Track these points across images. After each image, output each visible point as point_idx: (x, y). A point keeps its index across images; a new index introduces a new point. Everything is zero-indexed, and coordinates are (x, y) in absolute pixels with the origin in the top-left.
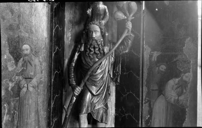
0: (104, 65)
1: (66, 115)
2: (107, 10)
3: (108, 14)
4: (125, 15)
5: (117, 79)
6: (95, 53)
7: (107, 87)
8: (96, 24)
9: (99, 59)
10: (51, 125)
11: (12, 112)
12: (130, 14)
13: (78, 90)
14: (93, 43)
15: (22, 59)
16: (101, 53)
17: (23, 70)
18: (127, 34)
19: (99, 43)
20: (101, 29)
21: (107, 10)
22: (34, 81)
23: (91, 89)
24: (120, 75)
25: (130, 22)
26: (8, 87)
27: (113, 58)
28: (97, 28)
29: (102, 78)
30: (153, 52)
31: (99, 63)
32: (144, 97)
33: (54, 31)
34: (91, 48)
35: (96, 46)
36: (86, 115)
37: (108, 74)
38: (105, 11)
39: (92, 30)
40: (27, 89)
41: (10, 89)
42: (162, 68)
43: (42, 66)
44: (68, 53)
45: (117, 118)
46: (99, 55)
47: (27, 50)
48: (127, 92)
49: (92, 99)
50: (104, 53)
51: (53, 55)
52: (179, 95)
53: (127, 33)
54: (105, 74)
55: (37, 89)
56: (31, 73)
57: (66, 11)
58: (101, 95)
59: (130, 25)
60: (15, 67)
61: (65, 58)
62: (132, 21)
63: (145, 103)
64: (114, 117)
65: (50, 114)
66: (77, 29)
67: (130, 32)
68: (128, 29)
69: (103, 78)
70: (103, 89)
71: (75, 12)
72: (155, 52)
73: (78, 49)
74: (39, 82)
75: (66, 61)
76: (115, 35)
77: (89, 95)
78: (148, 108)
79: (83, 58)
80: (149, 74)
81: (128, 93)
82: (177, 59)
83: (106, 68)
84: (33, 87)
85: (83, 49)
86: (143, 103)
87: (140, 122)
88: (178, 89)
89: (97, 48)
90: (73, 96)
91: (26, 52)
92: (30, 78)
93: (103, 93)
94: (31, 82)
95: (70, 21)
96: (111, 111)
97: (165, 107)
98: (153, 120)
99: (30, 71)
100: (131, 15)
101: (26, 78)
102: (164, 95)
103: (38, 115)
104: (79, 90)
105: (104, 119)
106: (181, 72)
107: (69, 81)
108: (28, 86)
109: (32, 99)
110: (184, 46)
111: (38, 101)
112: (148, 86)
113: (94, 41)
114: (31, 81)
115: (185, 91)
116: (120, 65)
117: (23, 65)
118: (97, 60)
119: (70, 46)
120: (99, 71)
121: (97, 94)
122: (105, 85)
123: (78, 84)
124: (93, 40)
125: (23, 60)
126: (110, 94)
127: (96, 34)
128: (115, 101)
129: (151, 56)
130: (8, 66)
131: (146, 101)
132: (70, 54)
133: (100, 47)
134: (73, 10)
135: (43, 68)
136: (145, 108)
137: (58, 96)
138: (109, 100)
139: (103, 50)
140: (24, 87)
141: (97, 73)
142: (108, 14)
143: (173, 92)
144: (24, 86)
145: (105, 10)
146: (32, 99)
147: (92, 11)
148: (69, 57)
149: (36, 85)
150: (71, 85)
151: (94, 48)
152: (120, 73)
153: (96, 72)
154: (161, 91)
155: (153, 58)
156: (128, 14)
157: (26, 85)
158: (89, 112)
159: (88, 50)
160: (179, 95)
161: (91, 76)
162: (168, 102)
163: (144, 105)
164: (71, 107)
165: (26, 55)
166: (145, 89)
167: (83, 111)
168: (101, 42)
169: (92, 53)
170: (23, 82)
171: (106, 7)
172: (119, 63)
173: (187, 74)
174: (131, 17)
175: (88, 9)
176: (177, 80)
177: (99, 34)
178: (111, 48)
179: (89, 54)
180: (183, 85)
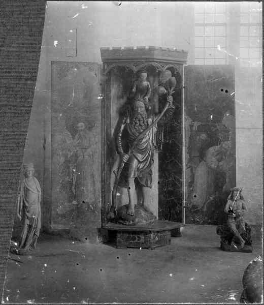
2: (150, 87)
4: (167, 89)
5: (160, 146)
9: (144, 130)
12: (171, 88)
16: (145, 125)
19: (143, 116)
38: (148, 85)
47: (82, 126)
50: (148, 125)
52: (219, 161)
55: (92, 157)
59: (170, 99)
60: (72, 141)
62: (173, 95)
66: (123, 101)
68: (170, 102)
71: (119, 85)
72: (196, 122)
73: (124, 121)
77: (135, 161)
80: (186, 79)
91: (80, 129)
92: (86, 149)
100: (172, 89)
102: (205, 161)
107: (117, 150)
113: (139, 116)
118: (142, 131)
120: (144, 140)
123: (126, 152)
124: (138, 115)
139: (147, 122)
140: (80, 156)
141: (142, 142)
145: (148, 85)
148: (115, 127)
150: (119, 153)
153: (141, 142)
154: (202, 156)
156: (169, 89)
158: (136, 176)
160: (219, 161)
161: (137, 145)
169: (137, 125)
173: (226, 142)
174: (172, 92)
177: (143, 109)
180: (221, 155)
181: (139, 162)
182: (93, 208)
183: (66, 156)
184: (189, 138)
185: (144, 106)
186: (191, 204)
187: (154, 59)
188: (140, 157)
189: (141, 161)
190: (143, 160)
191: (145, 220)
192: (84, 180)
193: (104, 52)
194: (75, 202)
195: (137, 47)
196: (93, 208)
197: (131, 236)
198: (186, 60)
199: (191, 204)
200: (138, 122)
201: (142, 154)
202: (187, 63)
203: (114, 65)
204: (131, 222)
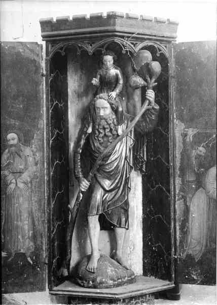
0: (119, 150)
1: (72, 216)
2: (120, 76)
3: (121, 82)
4: (146, 80)
6: (105, 134)
7: (126, 180)
10: (52, 230)
13: (85, 185)
14: (101, 123)
15: (7, 151)
19: (110, 122)
21: (120, 76)
22: (26, 176)
23: (102, 183)
24: (145, 161)
25: (152, 91)
27: (132, 140)
29: (117, 166)
30: (187, 130)
32: (177, 191)
33: (50, 112)
34: (99, 130)
35: (107, 126)
36: (98, 216)
37: (126, 161)
38: (117, 75)
40: (15, 185)
43: (36, 157)
45: (146, 221)
46: (110, 138)
47: (13, 139)
48: (156, 184)
50: (118, 135)
51: (51, 142)
53: (148, 105)
55: (30, 185)
56: (20, 167)
57: (69, 74)
58: (116, 190)
61: (70, 142)
62: (154, 89)
63: (178, 200)
65: (50, 216)
66: (85, 101)
67: (153, 103)
68: (149, 100)
69: (118, 167)
71: (81, 79)
75: (72, 145)
78: (182, 206)
79: (91, 142)
81: (157, 186)
84: (24, 183)
85: (90, 130)
86: (176, 200)
90: (79, 193)
91: (12, 142)
93: (120, 187)
94: (20, 177)
96: (137, 211)
98: (190, 222)
99: (19, 164)
100: (153, 80)
102: (204, 189)
104: (87, 184)
108: (18, 181)
109: (23, 196)
111: (31, 200)
112: (183, 175)
114: (20, 176)
116: (145, 147)
120: (112, 158)
121: (110, 188)
122: (122, 176)
125: (9, 151)
129: (185, 135)
132: (77, 135)
133: (112, 128)
134: (79, 75)
135: (37, 159)
136: (179, 206)
137: (60, 192)
140: (11, 183)
142: (121, 82)
144: (12, 181)
145: (117, 75)
146: (23, 196)
149: (29, 180)
152: (145, 159)
154: (200, 183)
155: (188, 137)
156: (149, 79)
157: (14, 181)
159: (97, 132)
165: (12, 146)
166: (178, 181)
168: (113, 121)
169: (101, 135)
171: (118, 72)
172: (143, 144)
174: (153, 83)
179: (98, 137)
181: (106, 191)
182: (31, 262)
184: (181, 153)
185: (108, 106)
186: (185, 253)
187: (115, 31)
188: (107, 184)
189: (107, 189)
190: (112, 187)
191: (111, 280)
192: (17, 221)
196: (31, 262)
198: (174, 35)
199: (185, 253)
201: (109, 179)
203: (61, 45)
204: (91, 282)
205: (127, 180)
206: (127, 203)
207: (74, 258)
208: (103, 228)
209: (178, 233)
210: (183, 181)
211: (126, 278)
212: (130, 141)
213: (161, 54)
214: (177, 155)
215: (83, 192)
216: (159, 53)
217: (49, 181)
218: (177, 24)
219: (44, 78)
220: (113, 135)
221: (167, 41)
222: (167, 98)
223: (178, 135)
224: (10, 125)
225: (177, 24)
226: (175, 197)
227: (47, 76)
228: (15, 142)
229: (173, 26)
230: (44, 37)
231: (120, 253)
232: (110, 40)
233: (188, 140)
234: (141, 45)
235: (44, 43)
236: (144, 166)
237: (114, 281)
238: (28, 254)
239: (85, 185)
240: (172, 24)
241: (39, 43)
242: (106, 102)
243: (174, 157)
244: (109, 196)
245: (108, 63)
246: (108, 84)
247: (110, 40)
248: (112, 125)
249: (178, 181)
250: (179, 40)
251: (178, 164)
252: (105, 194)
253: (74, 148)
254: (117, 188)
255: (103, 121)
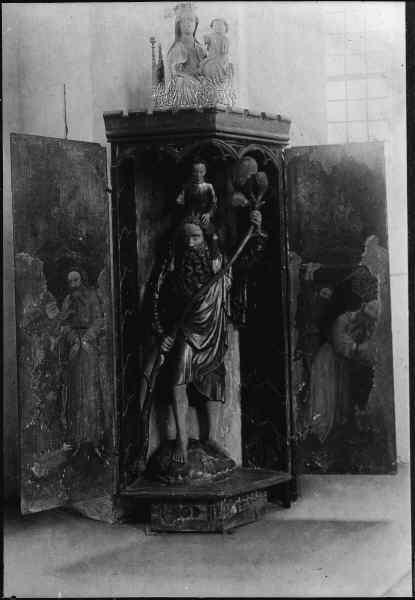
2: (213, 192)
4: (248, 198)
8: (195, 223)
9: (205, 284)
11: (58, 386)
13: (168, 343)
17: (71, 316)
18: (254, 235)
20: (204, 230)
22: (91, 332)
26: (49, 346)
28: (196, 229)
29: (212, 316)
31: (203, 292)
36: (185, 386)
39: (187, 233)
41: (52, 348)
42: (325, 293)
44: (144, 273)
49: (194, 357)
54: (216, 309)
58: (211, 349)
60: (58, 311)
62: (261, 210)
63: (295, 360)
64: (239, 389)
70: (212, 339)
74: (99, 332)
76: (234, 233)
78: (301, 370)
82: (352, 275)
83: (216, 300)
87: (288, 396)
88: (357, 332)
89: (198, 264)
95: (146, 215)
97: (102, 370)
100: (260, 198)
101: (77, 328)
103: (101, 391)
105: (219, 393)
106: (360, 300)
110: (363, 251)
114: (85, 332)
115: (368, 333)
117: (71, 307)
119: (147, 261)
120: (205, 305)
122: (217, 332)
125: (71, 298)
126: (227, 347)
127: (195, 240)
128: (238, 359)
129: (303, 271)
130: (47, 311)
131: (298, 355)
136: (296, 367)
138: (226, 357)
140: (74, 343)
141: (201, 309)
143: (347, 336)
147: (186, 198)
151: (194, 265)
154: (325, 336)
155: (307, 274)
156: (253, 196)
157: (77, 339)
162: (339, 355)
163: (293, 364)
164: (156, 374)
165: (76, 288)
166: (294, 334)
167: (178, 378)
168: (206, 254)
169: (189, 274)
170: (73, 336)
171: (211, 186)
174: (259, 201)
175: (177, 197)
176: (354, 314)
177: (200, 240)
178: (226, 261)
181: (196, 351)
183: (47, 350)
185: (200, 232)
189: (199, 348)
193: (109, 119)
194: (66, 447)
195: (109, 119)
197: (181, 507)
200: (190, 268)
201: (201, 333)
202: (289, 142)
205: (224, 335)
206: (222, 368)
207: (153, 443)
208: (191, 404)
209: (295, 406)
210: (300, 334)
211: (227, 470)
212: (228, 281)
213: (270, 162)
214: (292, 300)
215: (165, 353)
216: (267, 160)
217: (118, 340)
218: (289, 122)
219: (110, 195)
220: (206, 272)
221: (277, 144)
222: (17, 313)
223: (293, 271)
224: (71, 259)
225: (289, 122)
226: (290, 357)
227: (113, 192)
228: (78, 283)
229: (284, 124)
230: (108, 136)
231: (214, 437)
232: (207, 141)
233: (307, 278)
234: (245, 150)
235: (108, 146)
236: (244, 316)
237: (213, 474)
238: (96, 444)
239: (168, 343)
240: (283, 122)
241: (102, 145)
242: (198, 228)
243: (288, 303)
244: (201, 358)
245: (200, 174)
246: (198, 203)
247: (207, 141)
248: (205, 259)
249: (294, 334)
250: (291, 144)
251: (293, 309)
252: (194, 357)
253: (145, 295)
254: (212, 345)
255: (192, 253)
